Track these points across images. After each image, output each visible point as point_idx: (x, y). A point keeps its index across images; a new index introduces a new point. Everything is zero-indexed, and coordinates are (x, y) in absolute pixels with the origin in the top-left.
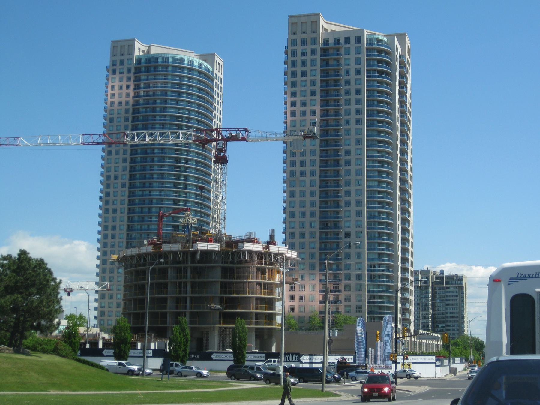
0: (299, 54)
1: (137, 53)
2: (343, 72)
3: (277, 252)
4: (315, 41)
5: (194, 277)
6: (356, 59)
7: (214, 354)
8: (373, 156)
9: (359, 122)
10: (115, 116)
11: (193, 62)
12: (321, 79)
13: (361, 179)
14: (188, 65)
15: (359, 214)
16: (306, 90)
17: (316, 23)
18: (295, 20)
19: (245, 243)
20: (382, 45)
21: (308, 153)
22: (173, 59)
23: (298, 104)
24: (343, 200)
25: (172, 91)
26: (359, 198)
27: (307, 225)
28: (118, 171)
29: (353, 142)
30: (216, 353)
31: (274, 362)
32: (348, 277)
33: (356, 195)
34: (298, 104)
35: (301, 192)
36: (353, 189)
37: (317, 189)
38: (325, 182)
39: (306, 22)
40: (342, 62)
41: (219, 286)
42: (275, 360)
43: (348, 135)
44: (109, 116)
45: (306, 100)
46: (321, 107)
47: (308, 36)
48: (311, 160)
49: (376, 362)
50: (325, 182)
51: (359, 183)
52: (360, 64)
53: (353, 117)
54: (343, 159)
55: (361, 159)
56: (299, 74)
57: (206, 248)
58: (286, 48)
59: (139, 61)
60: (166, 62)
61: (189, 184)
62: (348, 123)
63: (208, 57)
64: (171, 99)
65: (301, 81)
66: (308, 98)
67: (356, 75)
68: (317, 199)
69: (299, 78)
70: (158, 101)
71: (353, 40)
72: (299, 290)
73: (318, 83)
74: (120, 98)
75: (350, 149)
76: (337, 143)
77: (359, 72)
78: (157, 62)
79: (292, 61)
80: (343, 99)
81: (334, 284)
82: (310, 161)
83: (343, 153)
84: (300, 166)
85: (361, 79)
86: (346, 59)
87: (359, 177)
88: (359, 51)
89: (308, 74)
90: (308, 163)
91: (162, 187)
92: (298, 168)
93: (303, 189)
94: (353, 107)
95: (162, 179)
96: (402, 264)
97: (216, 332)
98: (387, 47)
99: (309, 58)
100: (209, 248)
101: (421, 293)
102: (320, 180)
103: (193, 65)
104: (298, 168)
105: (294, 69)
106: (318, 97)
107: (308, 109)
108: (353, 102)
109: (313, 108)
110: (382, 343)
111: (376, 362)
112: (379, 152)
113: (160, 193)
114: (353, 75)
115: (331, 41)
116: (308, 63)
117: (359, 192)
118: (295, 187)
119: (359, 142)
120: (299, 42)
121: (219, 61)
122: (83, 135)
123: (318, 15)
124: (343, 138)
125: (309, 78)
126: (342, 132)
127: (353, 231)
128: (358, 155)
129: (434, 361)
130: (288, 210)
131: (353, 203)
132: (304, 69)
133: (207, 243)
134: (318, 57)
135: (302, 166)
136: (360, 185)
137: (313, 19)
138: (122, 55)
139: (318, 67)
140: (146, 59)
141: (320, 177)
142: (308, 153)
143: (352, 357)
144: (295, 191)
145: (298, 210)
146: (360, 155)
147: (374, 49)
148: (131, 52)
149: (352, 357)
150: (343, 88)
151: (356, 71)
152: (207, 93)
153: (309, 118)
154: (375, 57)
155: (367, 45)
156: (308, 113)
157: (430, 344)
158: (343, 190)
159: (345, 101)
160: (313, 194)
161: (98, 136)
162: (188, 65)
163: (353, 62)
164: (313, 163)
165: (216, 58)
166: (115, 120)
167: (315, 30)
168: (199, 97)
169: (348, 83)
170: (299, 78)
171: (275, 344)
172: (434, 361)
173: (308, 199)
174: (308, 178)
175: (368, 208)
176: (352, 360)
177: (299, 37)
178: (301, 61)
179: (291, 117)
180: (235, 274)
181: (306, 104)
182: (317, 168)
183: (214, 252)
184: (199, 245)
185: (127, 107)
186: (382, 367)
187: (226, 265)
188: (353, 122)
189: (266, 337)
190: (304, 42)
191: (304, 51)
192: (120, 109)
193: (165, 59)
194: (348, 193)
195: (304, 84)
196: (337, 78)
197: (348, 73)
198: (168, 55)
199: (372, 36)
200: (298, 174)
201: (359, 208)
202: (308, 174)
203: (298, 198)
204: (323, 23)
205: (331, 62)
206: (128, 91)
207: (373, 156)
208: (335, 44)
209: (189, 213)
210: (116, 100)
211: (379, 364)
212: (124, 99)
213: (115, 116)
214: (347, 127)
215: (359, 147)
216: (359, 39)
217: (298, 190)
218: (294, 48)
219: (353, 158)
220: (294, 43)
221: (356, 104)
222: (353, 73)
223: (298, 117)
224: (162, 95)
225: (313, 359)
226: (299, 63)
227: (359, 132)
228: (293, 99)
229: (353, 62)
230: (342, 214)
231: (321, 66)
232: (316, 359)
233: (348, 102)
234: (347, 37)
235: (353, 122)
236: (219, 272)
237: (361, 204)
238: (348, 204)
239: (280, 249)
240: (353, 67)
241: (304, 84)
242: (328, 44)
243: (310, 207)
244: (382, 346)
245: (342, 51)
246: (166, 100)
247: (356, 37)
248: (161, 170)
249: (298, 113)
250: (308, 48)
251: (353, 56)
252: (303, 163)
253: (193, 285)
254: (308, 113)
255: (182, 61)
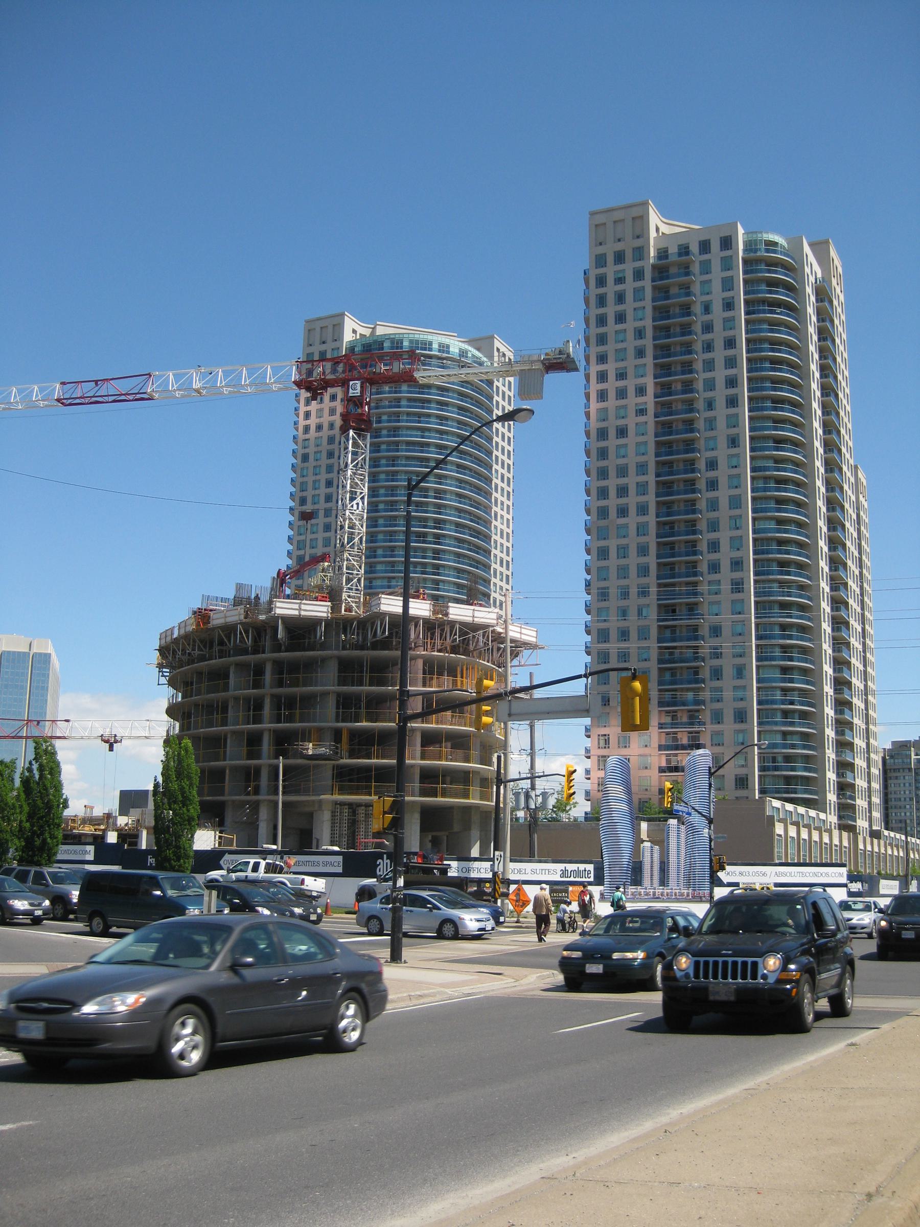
0: (610, 280)
1: (348, 337)
2: (698, 309)
3: (469, 619)
4: (640, 252)
5: (280, 684)
6: (723, 282)
7: (227, 857)
8: (766, 469)
9: (733, 402)
10: (311, 450)
11: (448, 347)
12: (654, 323)
13: (740, 516)
14: (439, 351)
15: (738, 586)
16: (625, 349)
17: (641, 220)
18: (601, 219)
19: (383, 596)
20: (775, 252)
21: (632, 470)
22: (411, 341)
23: (611, 376)
24: (704, 559)
25: (410, 399)
26: (736, 554)
27: (633, 612)
28: (316, 547)
29: (722, 442)
30: (232, 852)
31: (256, 868)
32: (718, 718)
33: (731, 548)
34: (611, 376)
35: (619, 548)
36: (724, 536)
37: (651, 540)
38: (667, 527)
39: (623, 220)
40: (696, 288)
41: (331, 703)
42: (259, 863)
43: (712, 429)
44: (301, 452)
45: (626, 368)
46: (655, 377)
47: (627, 246)
48: (637, 483)
49: (663, 882)
50: (667, 527)
51: (737, 523)
52: (731, 289)
53: (721, 394)
54: (702, 476)
55: (738, 476)
56: (611, 319)
57: (296, 613)
58: (585, 273)
59: (351, 349)
60: (397, 348)
61: (443, 566)
62: (710, 405)
63: (484, 343)
64: (408, 414)
65: (616, 331)
66: (631, 362)
67: (724, 311)
68: (652, 560)
69: (611, 327)
70: (385, 418)
71: (715, 246)
72: (619, 747)
73: (649, 333)
74: (320, 417)
75: (716, 457)
76: (689, 446)
77: (729, 305)
78: (383, 349)
79: (597, 295)
80: (699, 358)
81: (690, 733)
82: (637, 486)
83: (701, 465)
84: (618, 497)
85: (734, 317)
86: (703, 283)
87: (737, 512)
88: (728, 264)
89: (630, 316)
90: (632, 490)
91: (393, 572)
92: (613, 502)
93: (624, 541)
94: (720, 374)
95: (392, 556)
96: (835, 690)
97: (325, 812)
98: (788, 256)
99: (630, 286)
100: (303, 613)
101: (916, 780)
102: (658, 523)
103: (448, 352)
104: (613, 502)
105: (601, 311)
106: (649, 360)
107: (630, 384)
108: (720, 363)
109: (641, 381)
110: (683, 827)
111: (663, 882)
112: (777, 460)
113: (389, 582)
114: (718, 313)
115: (673, 250)
116: (629, 296)
117: (738, 543)
118: (608, 538)
119: (734, 442)
120: (610, 259)
121: (502, 349)
122: (63, 383)
123: (645, 204)
124: (701, 434)
125: (630, 325)
126: (700, 425)
127: (726, 618)
128: (732, 467)
129: (844, 880)
130: (596, 584)
131: (725, 565)
132: (620, 308)
133: (299, 601)
134: (647, 284)
135: (621, 497)
136: (738, 528)
137: (635, 212)
138: (324, 343)
139: (648, 303)
140: (363, 346)
141: (657, 516)
142: (632, 470)
143: (590, 867)
144: (608, 547)
145: (614, 585)
146: (736, 467)
147: (759, 261)
148: (338, 337)
149: (590, 867)
150: (699, 338)
151: (723, 304)
152: (476, 401)
153: (632, 400)
154: (761, 275)
155: (744, 253)
156: (631, 391)
157: (897, 857)
158: (704, 539)
159: (704, 364)
160: (643, 550)
161: (93, 383)
162: (439, 351)
163: (717, 286)
164: (642, 488)
165: (497, 344)
166: (311, 457)
167: (641, 233)
168: (461, 408)
169: (708, 328)
170: (611, 327)
171: (478, 843)
172: (844, 880)
173: (633, 560)
174: (632, 520)
175: (756, 574)
176: (592, 875)
177: (609, 250)
178: (615, 294)
179: (598, 402)
180: (366, 673)
181: (626, 376)
182: (651, 499)
183: (315, 622)
184: (278, 604)
185: (331, 433)
186: (682, 895)
187: (345, 653)
188: (720, 403)
189: (456, 828)
190: (620, 258)
191: (620, 275)
192: (318, 438)
193: (396, 343)
194: (714, 546)
195: (621, 337)
196: (686, 319)
197: (707, 309)
198: (401, 336)
199: (755, 236)
200: (613, 513)
201: (737, 575)
202: (633, 510)
203: (613, 562)
204: (655, 219)
205: (674, 291)
206: (333, 404)
207: (766, 469)
208: (680, 255)
209: (326, 564)
210: (313, 422)
211: (675, 885)
212: (326, 419)
213: (311, 450)
214: (710, 414)
215: (734, 451)
216: (727, 243)
217: (612, 544)
218: (601, 271)
219: (722, 473)
220: (600, 261)
221: (726, 369)
222: (717, 307)
223: (612, 402)
224: (390, 407)
225: (468, 870)
226: (611, 298)
227: (734, 421)
228: (602, 367)
229: (717, 286)
230: (704, 588)
231: (654, 300)
232: (479, 870)
233: (709, 365)
234: (703, 241)
235: (720, 403)
236: (332, 671)
237: (742, 567)
238: (715, 567)
239: (476, 614)
240: (717, 296)
241: (621, 337)
242: (667, 257)
243: (638, 576)
244: (683, 836)
245: (696, 268)
246: (398, 414)
247: (721, 238)
248: (391, 541)
249: (612, 394)
250: (628, 268)
251: (717, 274)
252: (622, 491)
253: (278, 702)
254: (631, 391)
255: (427, 345)
